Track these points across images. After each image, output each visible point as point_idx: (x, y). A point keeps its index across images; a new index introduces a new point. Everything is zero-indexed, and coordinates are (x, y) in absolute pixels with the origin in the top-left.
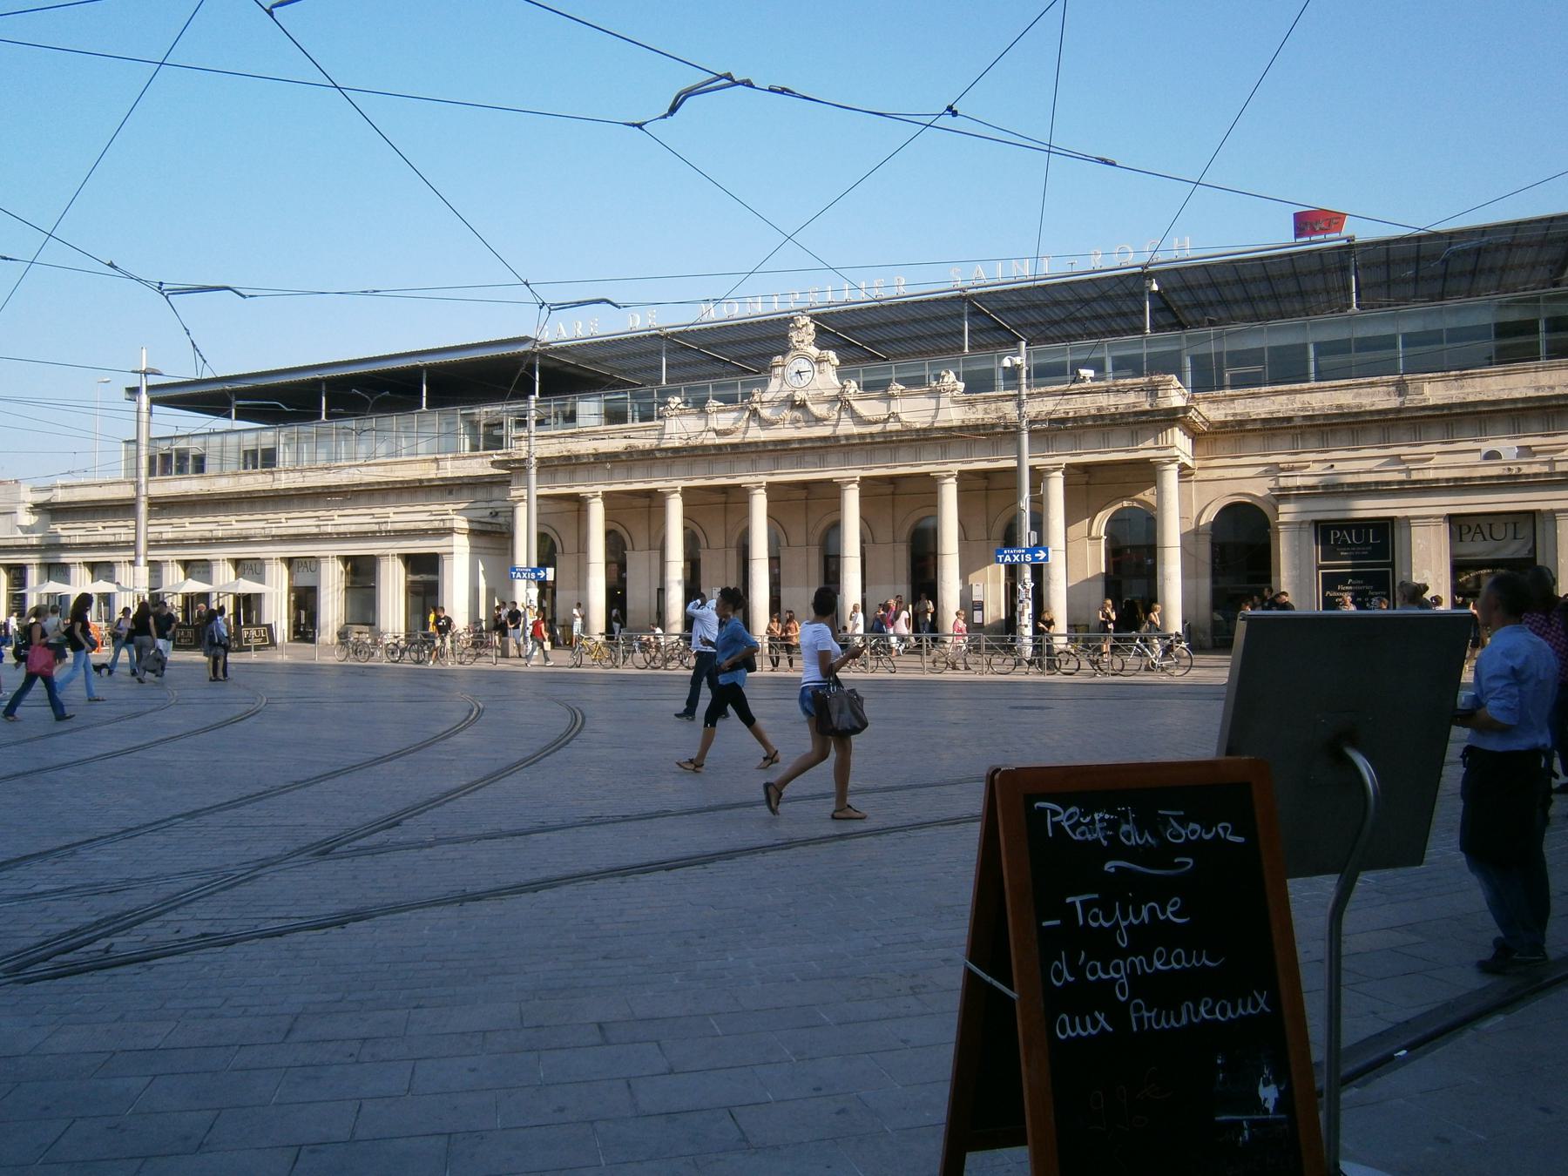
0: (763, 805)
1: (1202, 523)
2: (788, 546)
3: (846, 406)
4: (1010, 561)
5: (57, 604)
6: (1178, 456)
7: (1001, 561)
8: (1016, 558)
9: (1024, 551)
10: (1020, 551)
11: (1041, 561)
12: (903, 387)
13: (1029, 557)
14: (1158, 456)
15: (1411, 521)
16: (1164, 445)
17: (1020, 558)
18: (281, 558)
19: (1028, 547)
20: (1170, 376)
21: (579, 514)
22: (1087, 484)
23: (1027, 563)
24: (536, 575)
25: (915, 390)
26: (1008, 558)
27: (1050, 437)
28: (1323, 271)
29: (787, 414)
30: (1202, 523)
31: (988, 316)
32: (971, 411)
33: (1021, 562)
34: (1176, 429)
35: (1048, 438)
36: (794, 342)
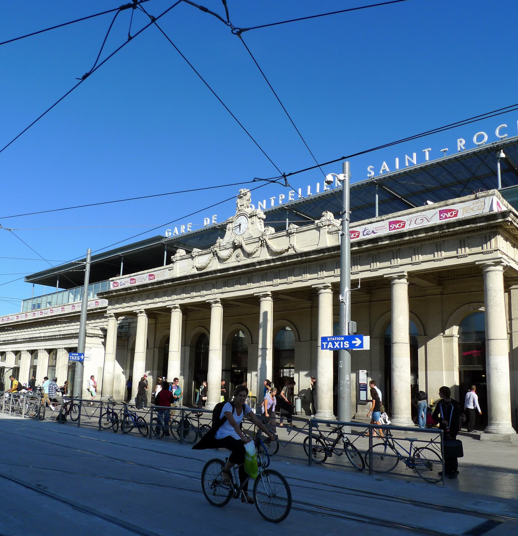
0: (293, 500)
2: (252, 343)
3: (264, 244)
6: (501, 258)
7: (325, 347)
9: (343, 339)
10: (339, 339)
12: (298, 227)
13: (347, 345)
14: (483, 259)
16: (489, 249)
17: (339, 345)
18: (45, 349)
19: (347, 334)
20: (492, 191)
21: (156, 326)
22: (442, 294)
23: (346, 349)
24: (350, 344)
25: (305, 228)
27: (395, 251)
31: (400, 199)
33: (340, 349)
34: (500, 236)
35: (393, 253)
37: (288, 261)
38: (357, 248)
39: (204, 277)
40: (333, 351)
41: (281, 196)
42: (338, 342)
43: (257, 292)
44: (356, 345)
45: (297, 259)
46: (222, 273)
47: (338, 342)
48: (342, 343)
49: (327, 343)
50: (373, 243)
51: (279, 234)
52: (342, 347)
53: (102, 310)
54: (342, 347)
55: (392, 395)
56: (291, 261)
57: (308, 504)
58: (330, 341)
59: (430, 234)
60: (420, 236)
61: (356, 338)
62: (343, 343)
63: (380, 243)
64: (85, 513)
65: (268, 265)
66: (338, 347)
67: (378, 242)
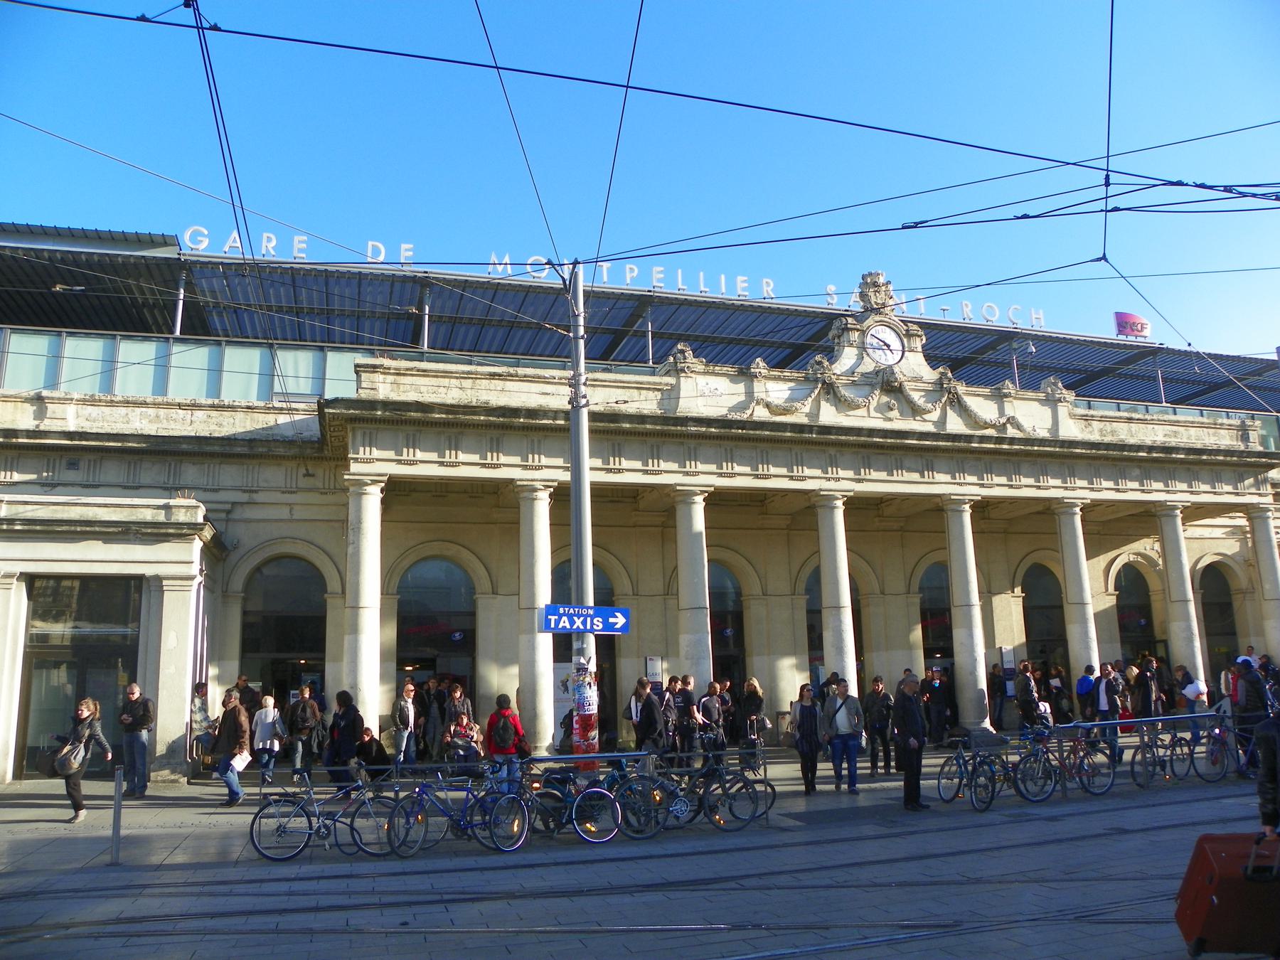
1: (1198, 568)
4: (568, 627)
5: (112, 802)
8: (578, 622)
10: (584, 612)
11: (617, 630)
14: (524, 477)
15: (165, 582)
17: (584, 623)
26: (565, 623)
28: (358, 318)
29: (878, 398)
30: (1198, 568)
32: (1087, 430)
36: (873, 303)
37: (1036, 448)
38: (1145, 454)
39: (833, 437)
40: (551, 634)
41: (631, 269)
42: (582, 619)
43: (972, 493)
44: (616, 627)
45: (1052, 449)
46: (886, 438)
47: (582, 619)
48: (589, 619)
49: (557, 617)
50: (1166, 453)
51: (981, 390)
52: (588, 627)
53: (32, 441)
54: (588, 627)
55: (1206, 654)
56: (1041, 448)
57: (364, 905)
58: (564, 614)
59: (1228, 459)
60: (1218, 458)
61: (616, 614)
62: (592, 621)
63: (1174, 456)
64: (105, 923)
65: (998, 446)
66: (582, 627)
67: (1171, 453)
